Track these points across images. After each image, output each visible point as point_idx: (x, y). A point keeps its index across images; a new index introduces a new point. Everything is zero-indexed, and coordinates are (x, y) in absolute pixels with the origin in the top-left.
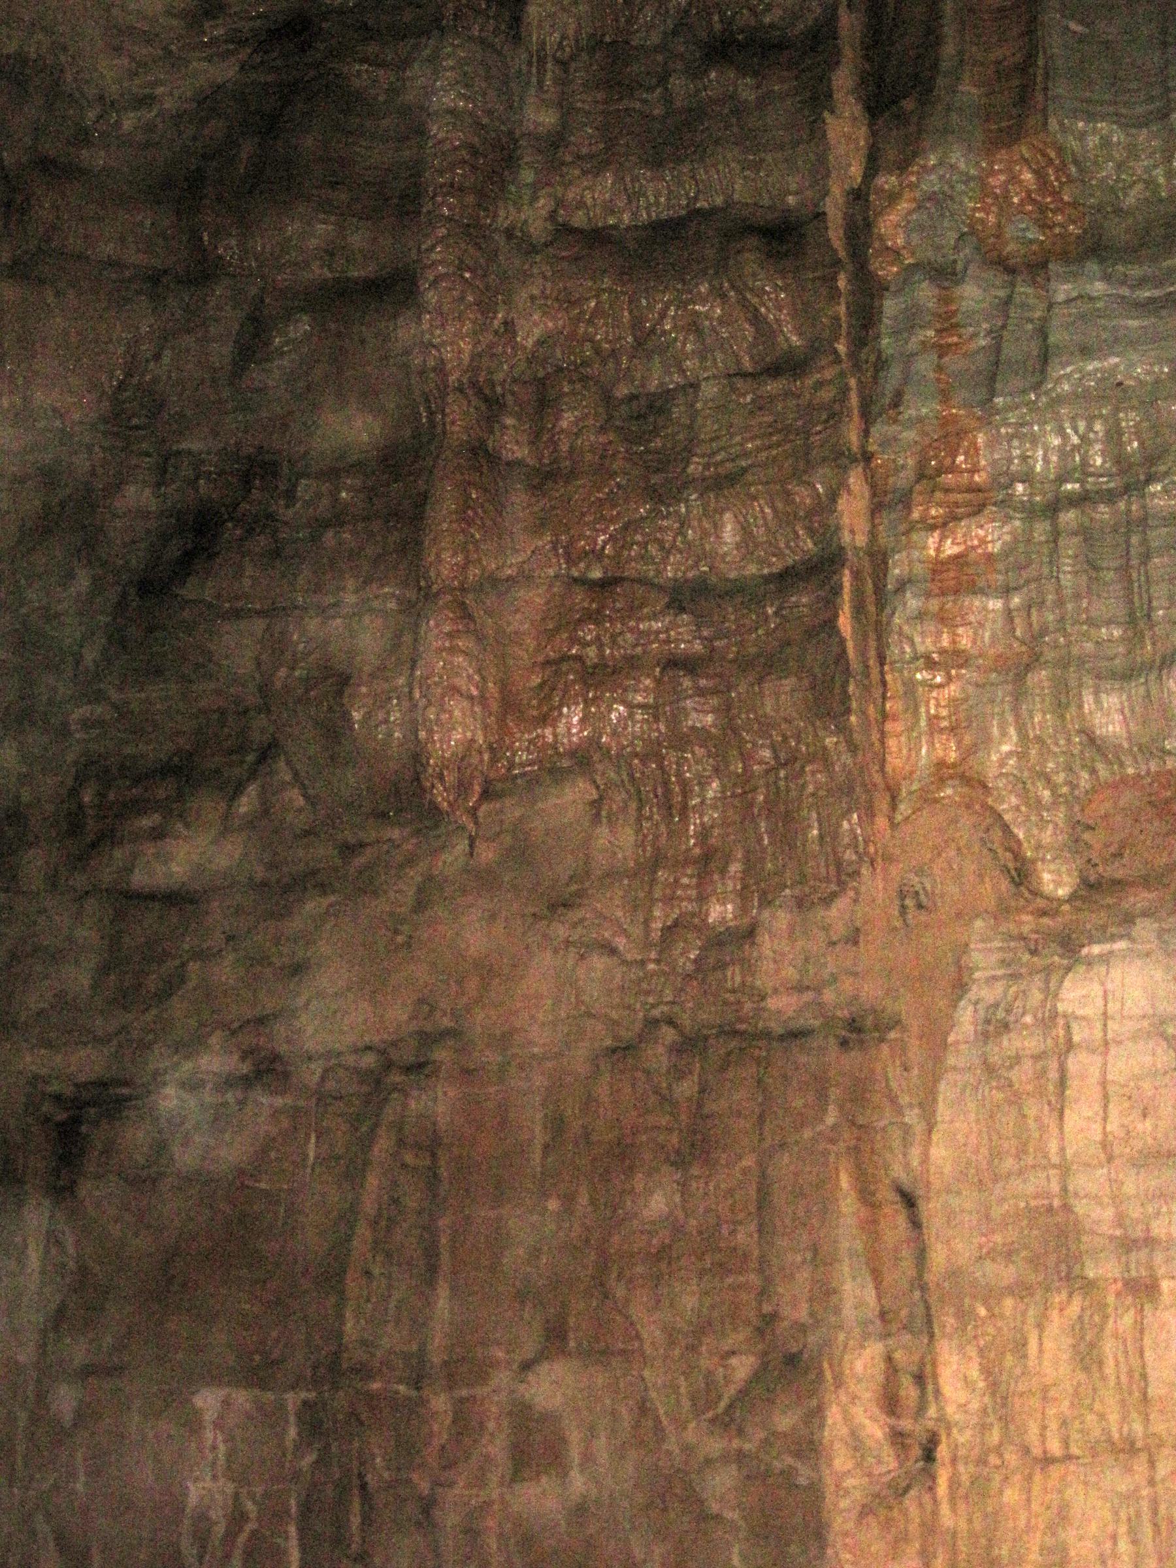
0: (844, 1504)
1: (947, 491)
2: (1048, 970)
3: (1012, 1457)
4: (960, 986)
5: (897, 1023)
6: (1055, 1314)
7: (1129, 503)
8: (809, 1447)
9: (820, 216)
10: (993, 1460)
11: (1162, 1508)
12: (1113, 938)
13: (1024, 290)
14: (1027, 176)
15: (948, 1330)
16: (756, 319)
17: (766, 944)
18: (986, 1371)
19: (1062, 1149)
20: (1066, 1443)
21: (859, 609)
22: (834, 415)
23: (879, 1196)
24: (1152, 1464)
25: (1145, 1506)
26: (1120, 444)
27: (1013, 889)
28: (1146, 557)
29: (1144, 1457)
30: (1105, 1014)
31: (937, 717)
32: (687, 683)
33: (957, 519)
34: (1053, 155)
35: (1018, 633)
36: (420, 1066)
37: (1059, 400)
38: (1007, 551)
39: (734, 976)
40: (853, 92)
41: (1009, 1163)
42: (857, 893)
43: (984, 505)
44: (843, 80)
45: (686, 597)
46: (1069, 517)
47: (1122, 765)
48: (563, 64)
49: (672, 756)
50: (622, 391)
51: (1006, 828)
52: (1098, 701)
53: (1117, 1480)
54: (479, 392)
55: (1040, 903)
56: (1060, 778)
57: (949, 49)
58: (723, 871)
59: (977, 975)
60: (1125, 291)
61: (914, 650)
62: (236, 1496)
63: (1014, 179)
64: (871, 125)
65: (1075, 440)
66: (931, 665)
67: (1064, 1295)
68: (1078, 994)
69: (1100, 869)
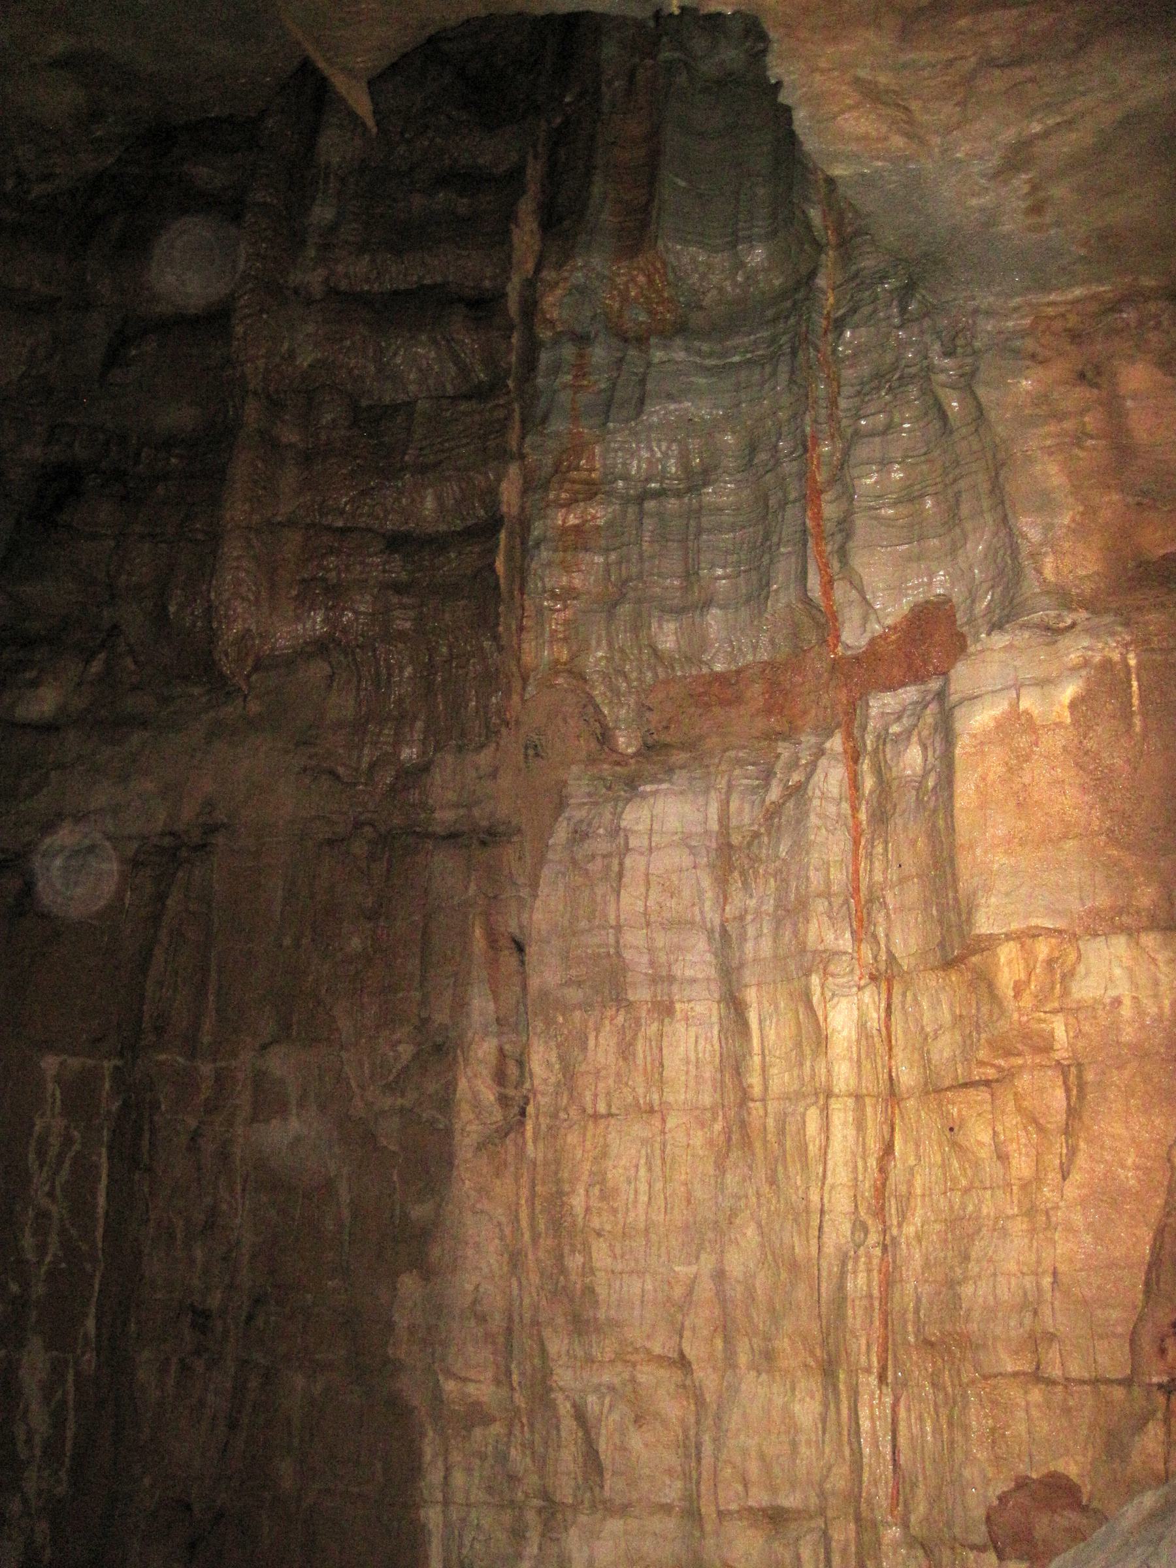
0: (467, 1141)
1: (574, 482)
2: (617, 799)
3: (573, 1112)
4: (561, 805)
5: (519, 831)
6: (607, 1022)
7: (690, 499)
8: (446, 1102)
9: (504, 295)
10: (563, 1115)
11: (668, 1150)
12: (661, 781)
13: (632, 352)
14: (641, 279)
15: (539, 1030)
16: (456, 360)
17: (437, 776)
18: (561, 1058)
19: (618, 916)
20: (610, 1106)
21: (510, 558)
22: (503, 426)
23: (500, 944)
24: (664, 1121)
25: (657, 1146)
26: (689, 461)
27: (598, 747)
28: (698, 535)
29: (658, 1115)
30: (651, 830)
31: (556, 631)
32: (395, 600)
33: (577, 501)
34: (659, 265)
35: (613, 578)
36: (204, 846)
37: (650, 427)
38: (610, 524)
39: (414, 796)
40: (534, 212)
41: (583, 924)
42: (498, 744)
43: (596, 494)
44: (527, 207)
45: (396, 542)
46: (650, 505)
47: (673, 668)
48: (343, 180)
49: (381, 648)
50: (364, 403)
51: (597, 707)
52: (660, 627)
53: (638, 1130)
54: (268, 396)
55: (615, 757)
56: (634, 675)
57: (596, 190)
58: (412, 727)
59: (572, 801)
60: (698, 360)
61: (544, 587)
62: (67, 1128)
63: (633, 279)
64: (543, 240)
65: (659, 455)
66: (554, 597)
67: (613, 1011)
68: (635, 817)
69: (655, 736)
